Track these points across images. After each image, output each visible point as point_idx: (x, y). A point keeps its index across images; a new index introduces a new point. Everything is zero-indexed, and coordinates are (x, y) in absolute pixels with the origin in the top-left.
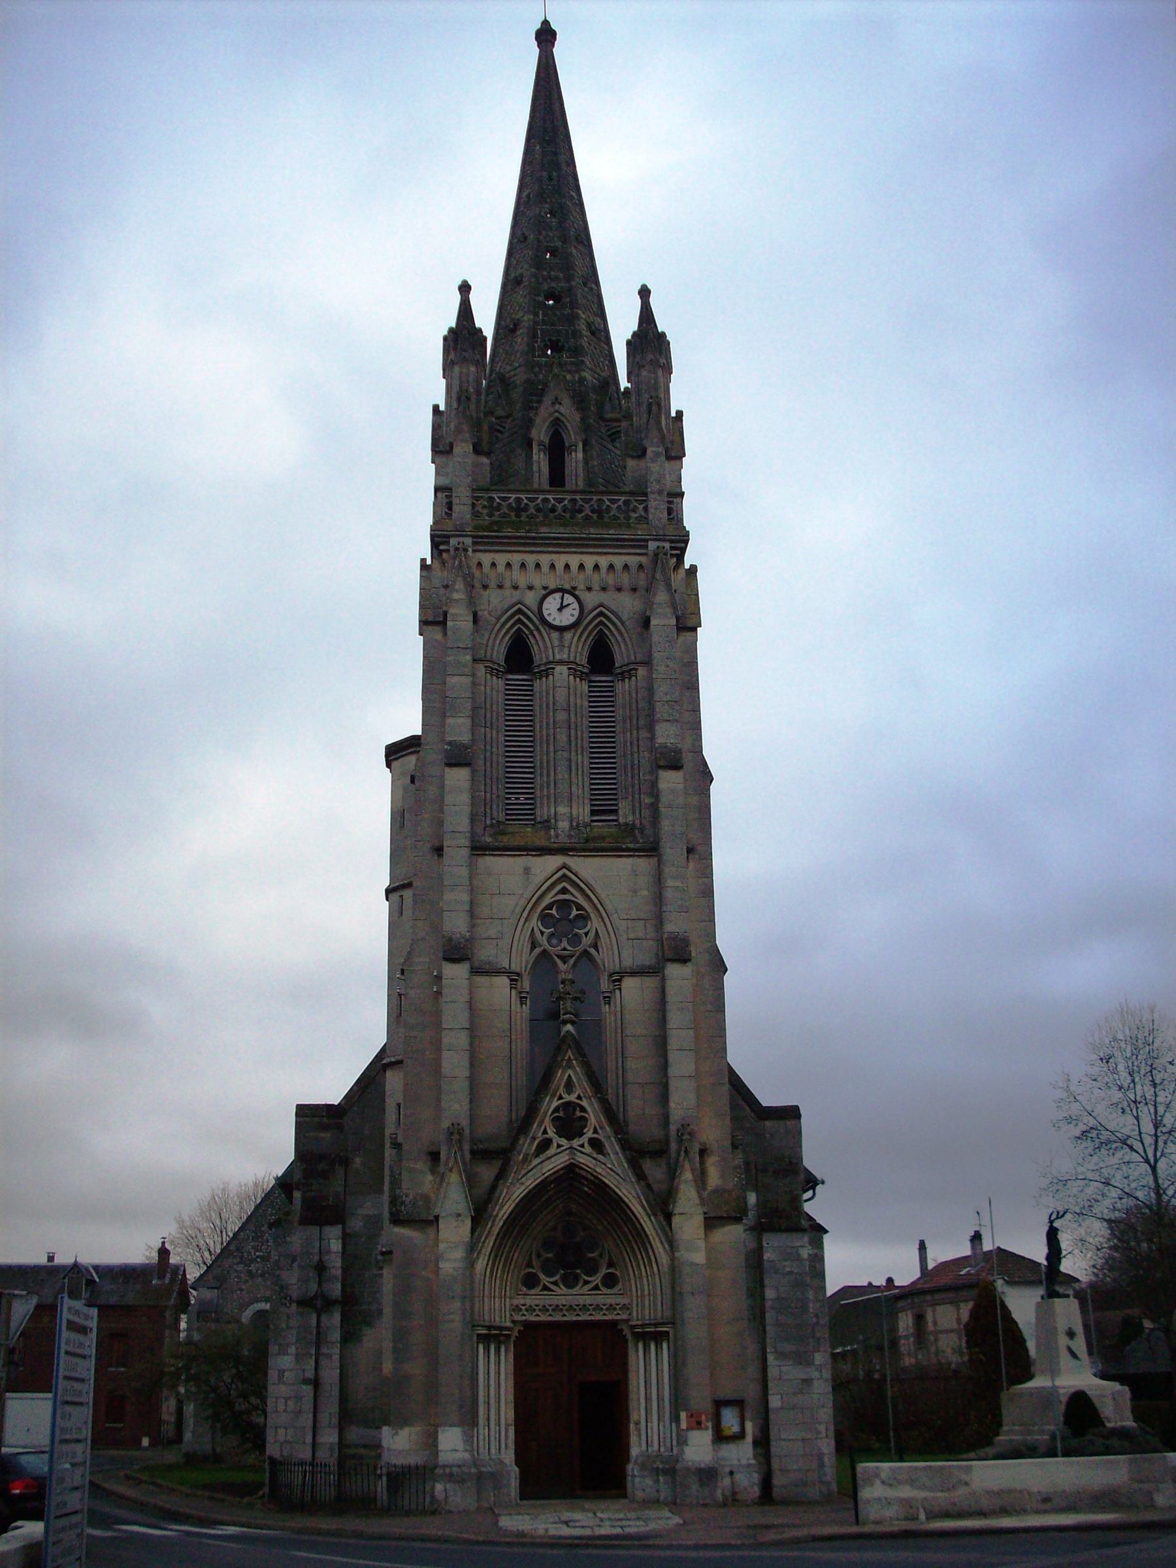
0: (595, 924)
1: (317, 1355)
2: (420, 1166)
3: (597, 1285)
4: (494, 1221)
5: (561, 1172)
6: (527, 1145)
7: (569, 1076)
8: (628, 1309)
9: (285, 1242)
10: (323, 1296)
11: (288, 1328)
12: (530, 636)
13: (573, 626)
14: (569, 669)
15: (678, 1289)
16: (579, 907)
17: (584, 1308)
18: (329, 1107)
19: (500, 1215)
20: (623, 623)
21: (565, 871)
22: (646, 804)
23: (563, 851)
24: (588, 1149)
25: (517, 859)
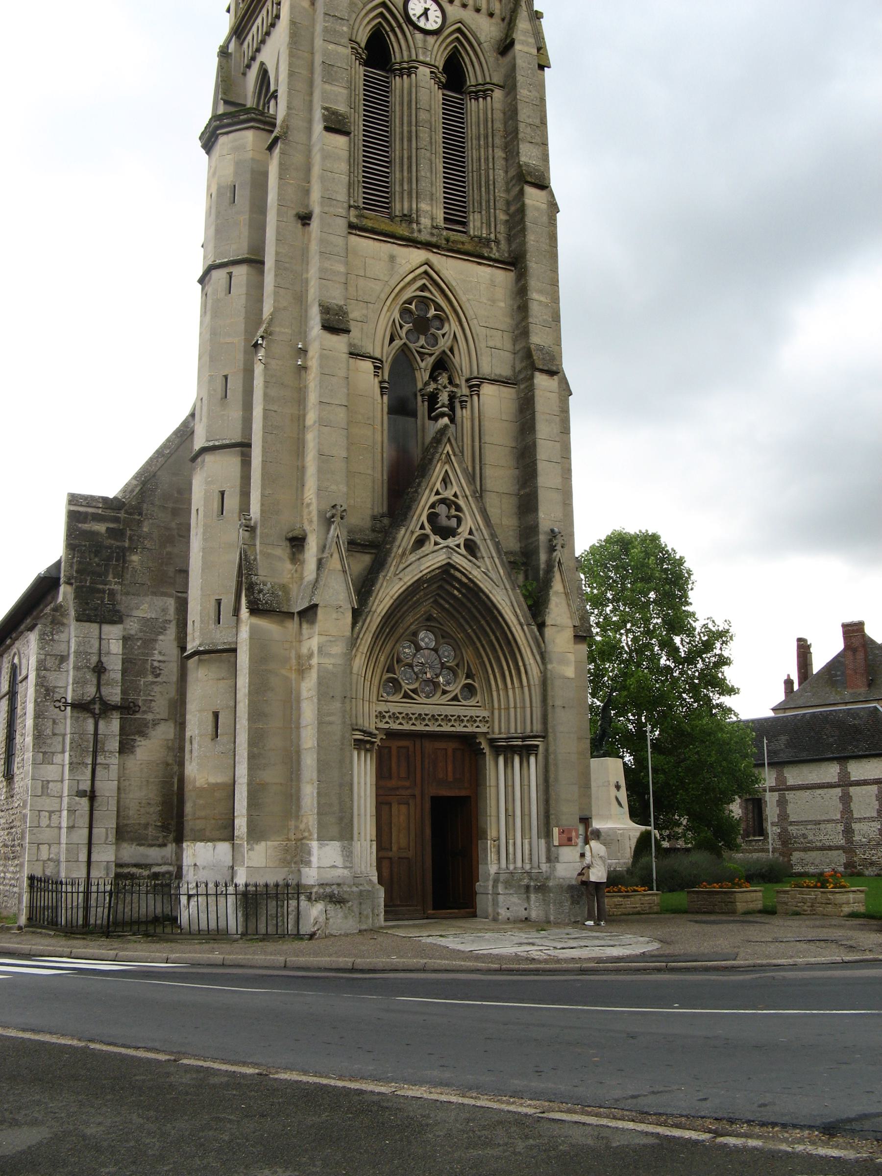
0: (452, 326)
1: (94, 765)
2: (278, 552)
3: (456, 695)
4: (373, 615)
5: (437, 571)
6: (405, 537)
7: (446, 471)
8: (487, 722)
9: (52, 640)
11: (54, 734)
12: (390, 33)
13: (436, 33)
14: (432, 72)
15: (550, 703)
16: (438, 307)
17: (447, 718)
18: (105, 500)
19: (378, 611)
20: (479, 44)
21: (426, 267)
22: (501, 220)
23: (427, 246)
24: (463, 551)
25: (383, 245)
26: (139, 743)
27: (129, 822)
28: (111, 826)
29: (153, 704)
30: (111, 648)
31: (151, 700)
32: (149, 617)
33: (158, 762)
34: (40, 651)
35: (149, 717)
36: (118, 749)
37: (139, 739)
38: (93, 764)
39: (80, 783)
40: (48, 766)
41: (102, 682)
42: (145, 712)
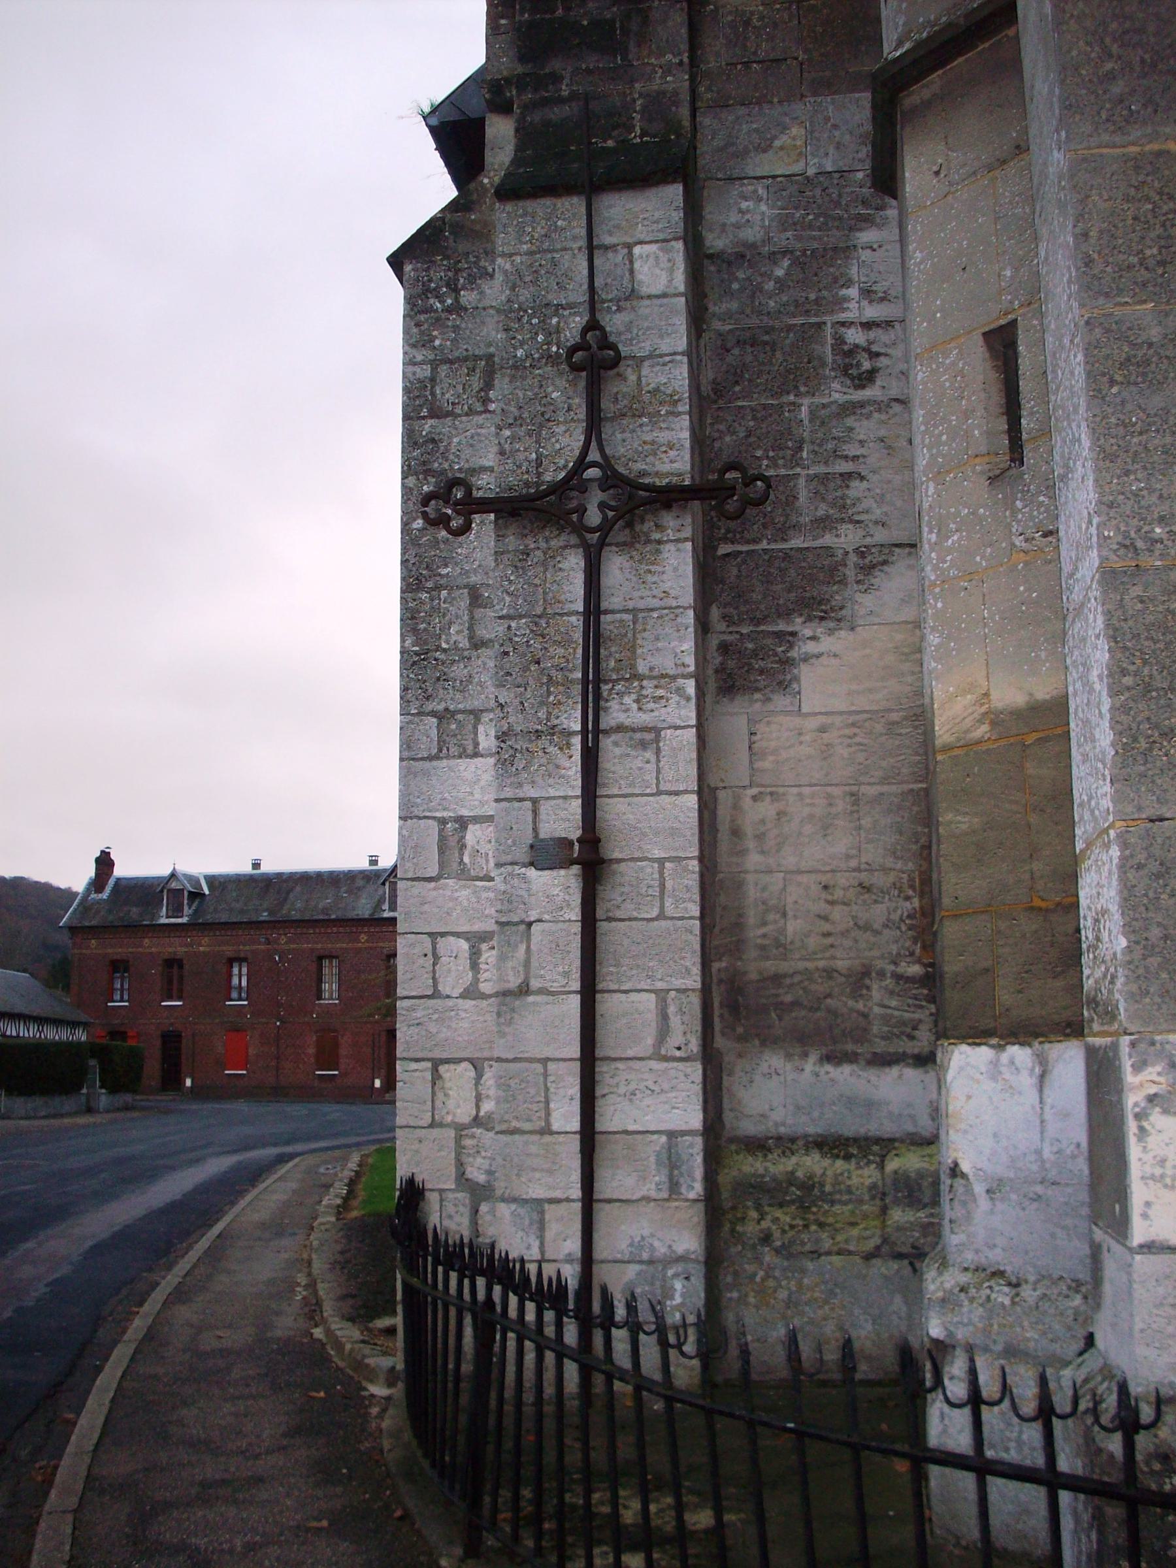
9: (458, 308)
10: (612, 479)
11: (477, 644)
26: (810, 647)
27: (784, 967)
28: (679, 983)
29: (856, 489)
30: (639, 277)
31: (847, 476)
32: (811, 172)
33: (895, 717)
34: (414, 352)
35: (846, 539)
36: (690, 660)
37: (808, 632)
38: (584, 731)
39: (544, 808)
40: (463, 763)
41: (606, 404)
42: (824, 524)
